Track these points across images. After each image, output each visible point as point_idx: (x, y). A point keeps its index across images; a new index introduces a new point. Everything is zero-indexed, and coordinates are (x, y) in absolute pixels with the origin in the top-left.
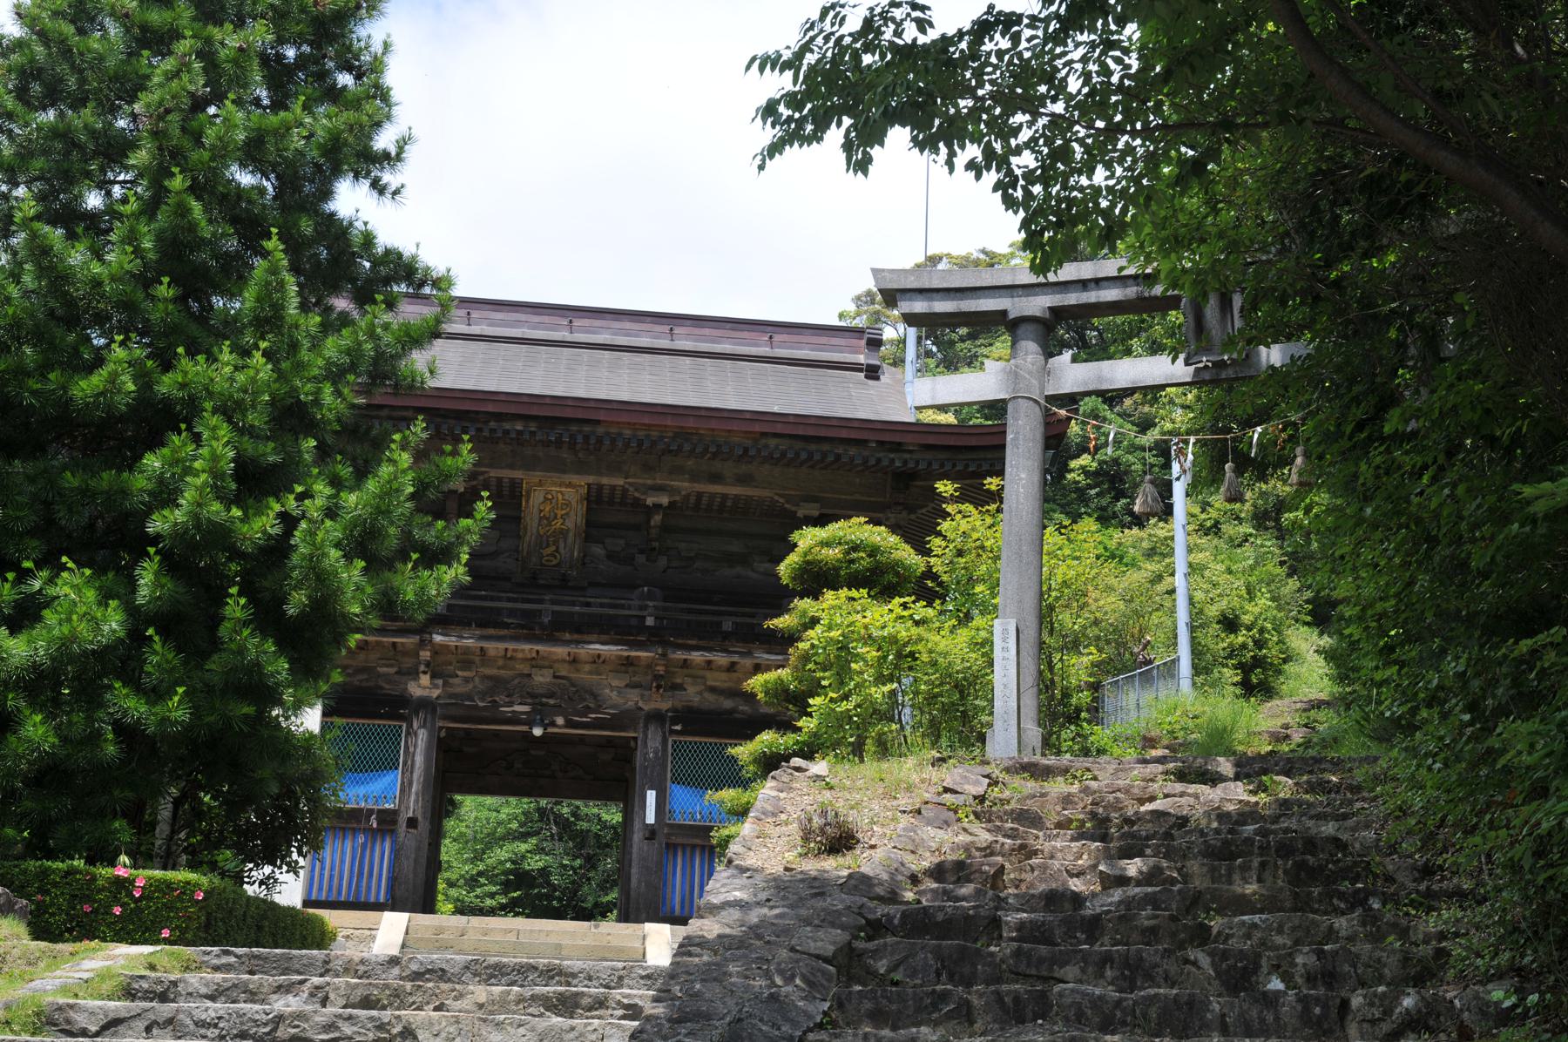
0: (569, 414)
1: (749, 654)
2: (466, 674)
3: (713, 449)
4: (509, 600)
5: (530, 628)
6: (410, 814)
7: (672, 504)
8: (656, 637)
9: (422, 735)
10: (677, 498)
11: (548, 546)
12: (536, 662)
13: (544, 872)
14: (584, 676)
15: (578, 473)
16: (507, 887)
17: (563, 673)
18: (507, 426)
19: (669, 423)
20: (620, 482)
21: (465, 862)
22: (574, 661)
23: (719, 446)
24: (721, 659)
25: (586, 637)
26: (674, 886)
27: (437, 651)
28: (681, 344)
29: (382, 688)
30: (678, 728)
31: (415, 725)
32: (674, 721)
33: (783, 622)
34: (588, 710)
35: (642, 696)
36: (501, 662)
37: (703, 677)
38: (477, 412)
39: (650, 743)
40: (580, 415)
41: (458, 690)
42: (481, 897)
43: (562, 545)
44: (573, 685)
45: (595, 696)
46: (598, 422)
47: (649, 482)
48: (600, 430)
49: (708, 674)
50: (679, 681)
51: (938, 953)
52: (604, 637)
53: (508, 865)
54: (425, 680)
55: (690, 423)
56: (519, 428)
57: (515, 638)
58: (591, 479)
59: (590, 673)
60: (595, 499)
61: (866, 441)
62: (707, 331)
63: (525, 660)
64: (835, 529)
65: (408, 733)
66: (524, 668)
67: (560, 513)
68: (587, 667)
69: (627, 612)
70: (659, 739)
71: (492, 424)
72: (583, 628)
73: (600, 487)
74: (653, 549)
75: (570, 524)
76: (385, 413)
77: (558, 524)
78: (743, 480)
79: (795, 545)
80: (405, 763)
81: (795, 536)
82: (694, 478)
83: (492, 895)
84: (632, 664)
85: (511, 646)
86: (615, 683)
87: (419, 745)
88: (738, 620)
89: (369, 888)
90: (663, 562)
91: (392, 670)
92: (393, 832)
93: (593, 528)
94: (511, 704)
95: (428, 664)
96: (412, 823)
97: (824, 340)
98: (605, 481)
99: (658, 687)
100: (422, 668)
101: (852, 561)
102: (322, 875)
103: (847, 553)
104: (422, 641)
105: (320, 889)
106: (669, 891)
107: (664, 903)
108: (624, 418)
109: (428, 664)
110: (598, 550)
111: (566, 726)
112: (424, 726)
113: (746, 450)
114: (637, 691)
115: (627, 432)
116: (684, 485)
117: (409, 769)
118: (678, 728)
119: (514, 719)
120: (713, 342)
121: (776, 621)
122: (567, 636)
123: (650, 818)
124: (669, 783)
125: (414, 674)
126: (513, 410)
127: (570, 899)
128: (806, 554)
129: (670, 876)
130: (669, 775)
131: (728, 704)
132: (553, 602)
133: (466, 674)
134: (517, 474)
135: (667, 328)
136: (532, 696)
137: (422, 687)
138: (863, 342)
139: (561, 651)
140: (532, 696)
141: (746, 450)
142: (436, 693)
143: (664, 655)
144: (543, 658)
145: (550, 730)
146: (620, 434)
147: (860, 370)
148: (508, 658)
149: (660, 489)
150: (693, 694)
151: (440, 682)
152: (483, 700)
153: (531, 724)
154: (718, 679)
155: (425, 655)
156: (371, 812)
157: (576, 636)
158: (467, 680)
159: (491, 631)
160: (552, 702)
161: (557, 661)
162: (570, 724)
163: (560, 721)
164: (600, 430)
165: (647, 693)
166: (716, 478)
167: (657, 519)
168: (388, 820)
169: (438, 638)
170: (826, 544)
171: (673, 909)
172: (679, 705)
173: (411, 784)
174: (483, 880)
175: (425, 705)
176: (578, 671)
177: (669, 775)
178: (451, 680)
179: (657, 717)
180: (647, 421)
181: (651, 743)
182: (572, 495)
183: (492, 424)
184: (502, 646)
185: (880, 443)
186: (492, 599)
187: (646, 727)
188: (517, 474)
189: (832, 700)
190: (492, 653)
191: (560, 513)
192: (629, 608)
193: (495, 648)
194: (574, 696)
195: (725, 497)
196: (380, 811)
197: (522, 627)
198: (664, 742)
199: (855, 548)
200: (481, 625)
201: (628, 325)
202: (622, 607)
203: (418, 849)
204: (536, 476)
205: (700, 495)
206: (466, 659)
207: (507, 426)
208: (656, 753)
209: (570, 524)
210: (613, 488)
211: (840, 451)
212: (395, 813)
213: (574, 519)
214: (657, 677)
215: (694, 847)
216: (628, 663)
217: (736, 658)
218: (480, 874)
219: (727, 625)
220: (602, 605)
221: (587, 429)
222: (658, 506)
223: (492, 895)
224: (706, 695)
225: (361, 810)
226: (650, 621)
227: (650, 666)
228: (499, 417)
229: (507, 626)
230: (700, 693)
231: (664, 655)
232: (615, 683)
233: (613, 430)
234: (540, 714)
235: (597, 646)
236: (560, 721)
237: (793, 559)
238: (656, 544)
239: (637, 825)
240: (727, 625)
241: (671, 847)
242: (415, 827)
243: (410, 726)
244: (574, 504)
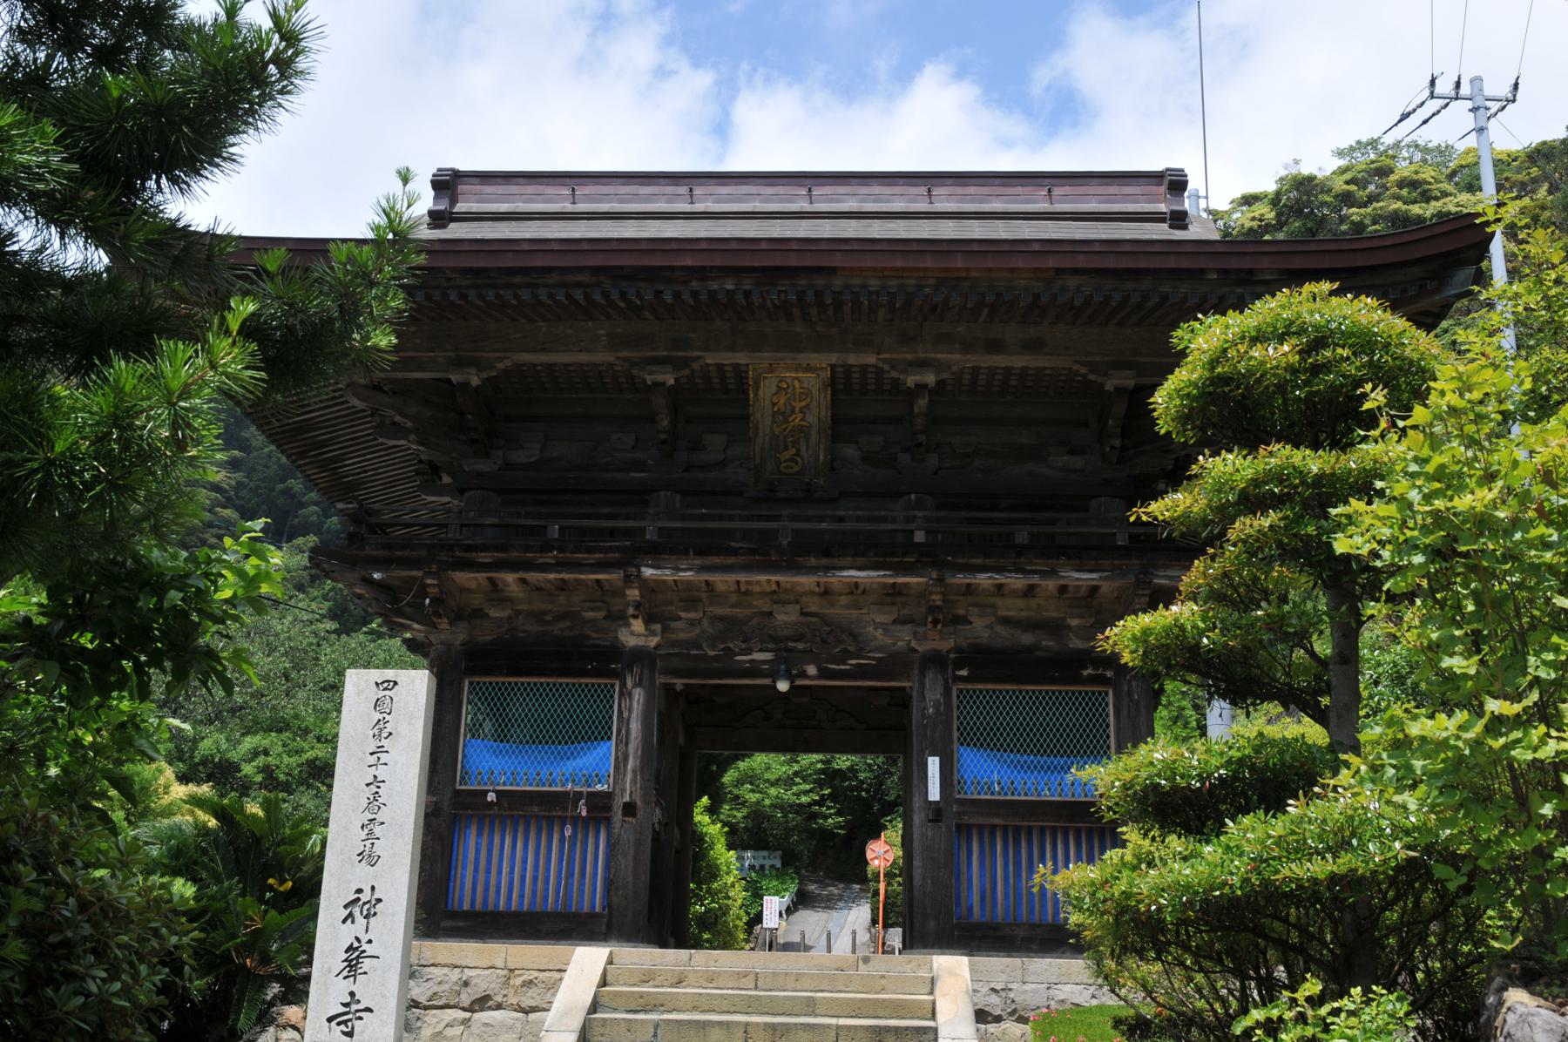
0: (793, 261)
1: (1053, 573)
2: (691, 615)
3: (990, 298)
4: (742, 519)
5: (764, 554)
6: (627, 799)
7: (941, 384)
8: (928, 557)
9: (638, 695)
10: (946, 376)
11: (786, 449)
12: (778, 596)
13: (851, 769)
14: (840, 611)
15: (816, 351)
16: (820, 784)
17: (813, 609)
18: (714, 285)
19: (929, 264)
20: (871, 359)
21: (782, 764)
22: (826, 592)
23: (999, 295)
24: (1016, 581)
25: (837, 562)
26: (970, 880)
27: (651, 589)
28: (941, 206)
29: (588, 638)
30: (964, 673)
31: (629, 683)
32: (959, 665)
33: (1169, 506)
34: (846, 654)
35: (915, 634)
36: (733, 598)
37: (993, 606)
38: (673, 268)
39: (928, 695)
40: (809, 261)
41: (681, 636)
42: (798, 795)
43: (803, 446)
44: (826, 623)
45: (854, 636)
46: (832, 271)
47: (909, 357)
48: (838, 282)
49: (999, 601)
50: (962, 612)
51: (810, 427)
52: (861, 560)
53: (819, 766)
54: (638, 625)
55: (959, 263)
56: (730, 287)
57: (747, 568)
58: (834, 358)
59: (847, 607)
60: (841, 385)
61: (1203, 271)
62: (972, 190)
63: (764, 594)
64: (1268, 309)
65: (621, 694)
66: (764, 605)
67: (798, 405)
68: (843, 600)
69: (890, 527)
70: (940, 689)
71: (695, 284)
72: (831, 550)
73: (848, 368)
74: (919, 445)
75: (811, 419)
76: (553, 279)
77: (796, 420)
78: (1034, 346)
79: (1183, 354)
80: (619, 731)
81: (1180, 336)
82: (967, 346)
83: (806, 793)
84: (900, 594)
85: (743, 577)
86: (880, 618)
87: (633, 708)
88: (1035, 529)
89: (581, 892)
90: (933, 460)
91: (600, 615)
92: (608, 820)
93: (840, 426)
94: (748, 651)
95: (638, 606)
96: (629, 809)
97: (1114, 190)
98: (853, 359)
99: (935, 622)
100: (631, 611)
101: (1317, 369)
102: (523, 878)
103: (1305, 352)
104: (627, 576)
105: (522, 896)
106: (964, 886)
107: (958, 904)
108: (868, 262)
109: (638, 606)
110: (850, 451)
111: (819, 677)
112: (639, 684)
113: (1037, 297)
114: (909, 627)
115: (874, 283)
116: (956, 358)
117: (623, 741)
118: (964, 673)
119: (754, 670)
120: (980, 202)
121: (1156, 507)
122: (813, 561)
123: (934, 794)
124: (956, 745)
125: (622, 619)
126: (718, 261)
127: (876, 792)
128: (1213, 363)
129: (964, 868)
130: (956, 734)
131: (1027, 639)
132: (795, 518)
133: (691, 615)
134: (741, 358)
135: (923, 190)
136: (773, 639)
137: (635, 634)
138: (1163, 189)
139: (806, 581)
140: (773, 639)
141: (1037, 297)
142: (653, 641)
143: (940, 580)
144: (786, 591)
145: (799, 682)
146: (864, 286)
147: (1163, 220)
148: (743, 593)
149: (923, 364)
150: (980, 629)
151: (658, 627)
152: (713, 647)
153: (775, 676)
154: (1012, 608)
155: (633, 594)
156: (579, 795)
157: (824, 561)
158: (692, 623)
159: (715, 560)
160: (800, 646)
161: (805, 594)
162: (824, 673)
163: (812, 670)
164: (838, 282)
165: (921, 630)
166: (996, 346)
167: (922, 403)
168: (600, 805)
169: (648, 572)
170: (1258, 338)
171: (970, 909)
172: (964, 643)
173: (626, 758)
174: (798, 780)
175: (641, 656)
176: (831, 605)
177: (956, 734)
178: (674, 625)
179: (935, 660)
180: (899, 264)
181: (930, 695)
182: (812, 382)
183: (695, 284)
184: (731, 578)
185: (1224, 272)
186: (721, 518)
187: (922, 674)
188: (741, 358)
189: (1497, 724)
190: (721, 587)
191: (798, 405)
192: (894, 520)
193: (722, 581)
194: (827, 638)
195: (1008, 370)
196: (589, 794)
197: (753, 552)
198: (947, 692)
199: (1320, 341)
200: (701, 552)
201: (877, 190)
202: (884, 520)
203: (638, 843)
204: (764, 358)
205: (976, 370)
206: (689, 596)
207: (714, 285)
208: (936, 707)
209: (811, 419)
210: (864, 368)
211: (1166, 288)
212: (608, 796)
213: (816, 412)
214: (933, 609)
215: (993, 828)
216: (895, 592)
217: (1035, 579)
218: (796, 774)
219: (1022, 537)
220: (858, 519)
221: (820, 282)
222: (921, 387)
223: (806, 793)
224: (999, 629)
225: (567, 793)
226: (919, 537)
227: (923, 594)
228: (701, 273)
229: (734, 552)
230: (990, 627)
231: (940, 580)
232: (880, 618)
233: (855, 281)
234: (787, 663)
235: (853, 573)
236: (812, 670)
237: (1181, 377)
238: (922, 438)
239: (917, 803)
240: (1022, 537)
241: (964, 830)
242: (633, 815)
243: (623, 685)
244: (815, 392)
